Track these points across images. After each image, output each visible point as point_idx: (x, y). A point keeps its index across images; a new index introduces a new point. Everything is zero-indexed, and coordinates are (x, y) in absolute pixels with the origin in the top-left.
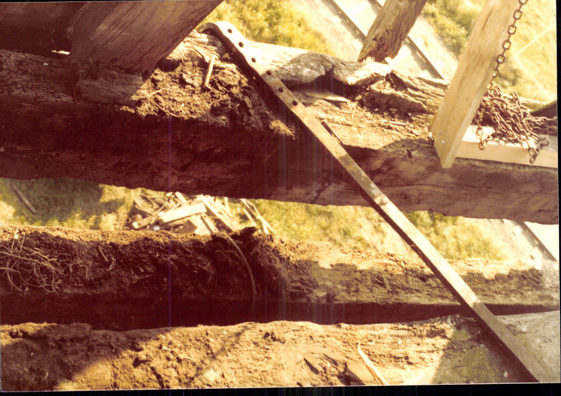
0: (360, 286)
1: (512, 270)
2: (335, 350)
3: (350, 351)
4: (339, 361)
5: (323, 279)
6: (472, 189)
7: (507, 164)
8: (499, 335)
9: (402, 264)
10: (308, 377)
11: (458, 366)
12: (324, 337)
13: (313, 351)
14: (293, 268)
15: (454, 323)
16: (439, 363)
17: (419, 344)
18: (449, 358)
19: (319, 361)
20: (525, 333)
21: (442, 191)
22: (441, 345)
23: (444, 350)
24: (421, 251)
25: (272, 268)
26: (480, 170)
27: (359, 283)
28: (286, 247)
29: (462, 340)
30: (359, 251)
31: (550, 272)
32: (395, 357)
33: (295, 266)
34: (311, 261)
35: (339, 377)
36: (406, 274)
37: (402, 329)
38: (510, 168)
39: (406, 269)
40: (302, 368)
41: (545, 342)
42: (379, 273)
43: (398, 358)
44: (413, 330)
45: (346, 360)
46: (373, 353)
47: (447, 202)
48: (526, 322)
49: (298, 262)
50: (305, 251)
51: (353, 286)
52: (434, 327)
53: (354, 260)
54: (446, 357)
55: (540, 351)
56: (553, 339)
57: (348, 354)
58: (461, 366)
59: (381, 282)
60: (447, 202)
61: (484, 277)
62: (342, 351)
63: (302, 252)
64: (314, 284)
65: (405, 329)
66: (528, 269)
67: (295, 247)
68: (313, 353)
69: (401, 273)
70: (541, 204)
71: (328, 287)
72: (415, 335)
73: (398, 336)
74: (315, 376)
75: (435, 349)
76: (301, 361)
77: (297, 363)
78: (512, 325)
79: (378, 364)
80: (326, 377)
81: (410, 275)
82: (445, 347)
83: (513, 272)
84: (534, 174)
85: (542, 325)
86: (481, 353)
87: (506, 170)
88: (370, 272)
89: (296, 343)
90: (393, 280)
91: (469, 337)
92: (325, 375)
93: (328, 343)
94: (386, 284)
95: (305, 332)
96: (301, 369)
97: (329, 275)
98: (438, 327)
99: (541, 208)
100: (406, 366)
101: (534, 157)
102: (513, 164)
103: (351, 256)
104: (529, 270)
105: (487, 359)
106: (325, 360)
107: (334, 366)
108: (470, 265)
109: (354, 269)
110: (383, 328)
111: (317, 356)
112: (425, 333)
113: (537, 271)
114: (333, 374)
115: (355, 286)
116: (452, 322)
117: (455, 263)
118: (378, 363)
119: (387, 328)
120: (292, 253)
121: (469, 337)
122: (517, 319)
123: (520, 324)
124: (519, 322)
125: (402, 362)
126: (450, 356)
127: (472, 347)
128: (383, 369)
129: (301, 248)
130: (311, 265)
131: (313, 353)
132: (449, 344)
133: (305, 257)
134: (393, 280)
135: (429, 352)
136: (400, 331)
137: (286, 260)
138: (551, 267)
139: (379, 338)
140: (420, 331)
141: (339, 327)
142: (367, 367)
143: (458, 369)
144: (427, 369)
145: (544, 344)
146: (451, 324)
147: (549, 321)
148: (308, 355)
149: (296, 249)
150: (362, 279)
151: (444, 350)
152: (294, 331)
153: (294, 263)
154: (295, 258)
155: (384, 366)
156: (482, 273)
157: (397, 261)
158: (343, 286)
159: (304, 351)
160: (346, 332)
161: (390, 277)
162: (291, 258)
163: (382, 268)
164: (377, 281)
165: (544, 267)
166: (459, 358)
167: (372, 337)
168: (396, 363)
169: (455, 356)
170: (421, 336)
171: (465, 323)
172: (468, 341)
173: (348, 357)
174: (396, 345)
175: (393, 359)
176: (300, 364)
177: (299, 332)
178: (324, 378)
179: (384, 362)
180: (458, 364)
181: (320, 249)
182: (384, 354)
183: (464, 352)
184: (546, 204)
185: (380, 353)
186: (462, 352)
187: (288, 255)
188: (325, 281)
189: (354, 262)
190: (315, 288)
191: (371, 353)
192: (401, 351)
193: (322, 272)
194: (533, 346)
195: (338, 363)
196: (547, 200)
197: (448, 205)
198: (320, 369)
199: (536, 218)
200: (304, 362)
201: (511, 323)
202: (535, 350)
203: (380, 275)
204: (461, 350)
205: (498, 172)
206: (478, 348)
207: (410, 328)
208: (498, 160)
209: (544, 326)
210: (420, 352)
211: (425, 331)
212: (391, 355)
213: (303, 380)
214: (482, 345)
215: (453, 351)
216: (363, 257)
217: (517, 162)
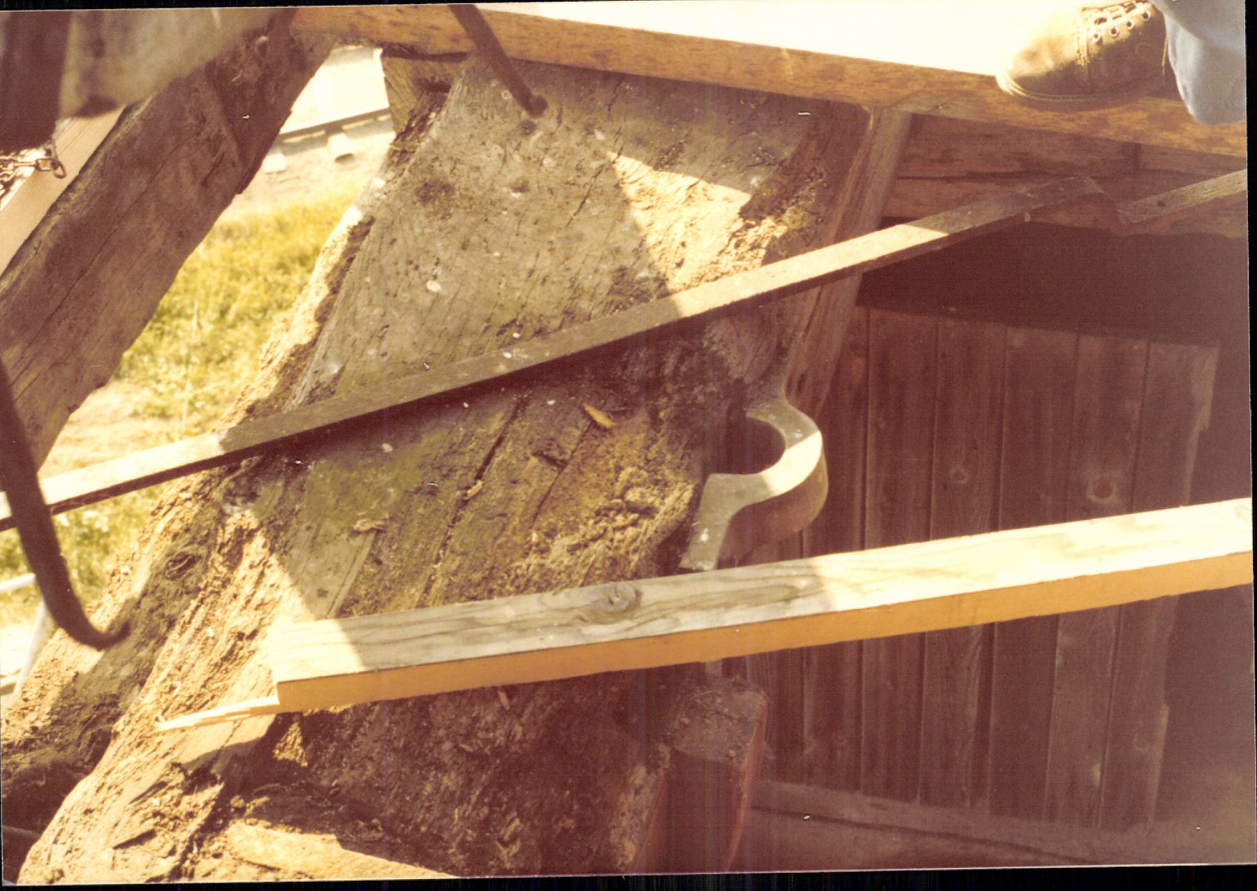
0: (167, 613)
1: (327, 277)
2: (139, 774)
3: (159, 743)
4: (162, 776)
5: (112, 678)
6: (64, 311)
7: (44, 221)
8: (306, 428)
9: (184, 495)
10: (148, 857)
11: (314, 538)
12: (103, 784)
13: (114, 821)
14: (56, 729)
15: (239, 500)
16: (287, 575)
17: (235, 596)
18: (291, 548)
19: (138, 818)
20: (342, 370)
21: (33, 376)
22: (260, 549)
23: (272, 551)
24: (68, 501)
25: (24, 778)
26: (23, 283)
27: (160, 610)
28: (11, 723)
29: (275, 502)
30: (113, 575)
31: (378, 199)
32: (225, 659)
33: (55, 723)
34: (69, 685)
35: (188, 790)
36: (204, 498)
37: (194, 613)
38: (56, 218)
39: (196, 494)
40: (126, 860)
41: (382, 338)
42: (168, 555)
43: (231, 652)
44: (207, 593)
45: (168, 759)
46: (190, 697)
47: (68, 372)
48: (325, 357)
49: (51, 713)
50: (42, 688)
51: (158, 625)
52: (223, 545)
53: (118, 596)
54: (285, 553)
55: (391, 358)
56: (388, 319)
57: (161, 751)
58: (318, 530)
59: (185, 562)
60: (68, 372)
61: (305, 346)
62: (148, 759)
63: (41, 696)
64: (108, 701)
65: (197, 608)
66: (345, 242)
67: (23, 704)
68: (116, 825)
69: (196, 508)
70: (186, 178)
71: (130, 677)
72: (218, 593)
73: (198, 630)
74: (155, 843)
75: (261, 568)
76: (114, 858)
77: (113, 866)
78: (314, 390)
79: (215, 699)
80: (171, 820)
81: (211, 490)
82: (269, 546)
83: (331, 279)
84: (102, 172)
85: (350, 328)
86: (321, 476)
87: (55, 228)
88: (157, 574)
89: (77, 850)
90: (197, 532)
91: (280, 484)
92: (166, 820)
93: (118, 782)
94: (195, 553)
95: (73, 819)
96: (126, 864)
97: (112, 664)
98: (227, 536)
99: (200, 179)
100: (254, 644)
101: (56, 164)
102: (53, 208)
103: (110, 596)
104: (349, 240)
105: (338, 471)
106: (144, 805)
107: (163, 790)
108: (270, 362)
109: (132, 605)
110: (172, 650)
111: (126, 817)
112: (224, 570)
113: (360, 223)
114: (174, 801)
115: (162, 620)
116: (234, 504)
117: (247, 391)
118: (213, 697)
119: (175, 641)
120: (31, 717)
121: (280, 484)
122: (309, 373)
123: (323, 372)
124: (316, 372)
125: (241, 648)
126: (289, 544)
127: (302, 490)
128: (227, 694)
129: (32, 694)
130: (74, 691)
131: (116, 825)
132: (266, 535)
133: (53, 694)
134: (197, 532)
135: (258, 583)
136: (193, 621)
137: (33, 737)
138: (372, 194)
139: (180, 669)
140: (215, 578)
141: (116, 734)
142: (198, 726)
143: (319, 539)
144: (282, 606)
145: (384, 344)
146: (236, 508)
147: (351, 310)
148: (113, 836)
149: (27, 705)
150: (159, 599)
151: (272, 551)
152: (55, 842)
153: (49, 722)
154: (41, 717)
155: (225, 688)
156: (295, 346)
157: (173, 505)
158: (147, 645)
159: (102, 841)
160: (129, 728)
161: (188, 536)
162: (39, 724)
163: (168, 542)
164: (180, 570)
165: (363, 206)
166: (304, 526)
167: (168, 683)
168: (237, 662)
169: (295, 535)
170: (226, 583)
171: (251, 479)
172: (285, 490)
173: (167, 754)
174: (211, 642)
175: (226, 665)
176: (118, 861)
177: (63, 833)
178: (172, 824)
179: (219, 684)
180: (310, 534)
181: (58, 655)
182: (205, 678)
183: (299, 510)
184: (194, 169)
185: (201, 683)
186: (297, 514)
187: (28, 727)
188: (117, 677)
189: (122, 600)
190: (115, 704)
191: (188, 703)
192: (223, 639)
193: (99, 673)
194: (374, 368)
195: (164, 779)
196: (184, 164)
197: (78, 371)
198: (149, 825)
199: (218, 197)
200: (119, 851)
201: (308, 389)
202: (383, 370)
203: (173, 557)
204: (293, 513)
205: (51, 245)
206: (309, 477)
207: (200, 596)
208: (26, 236)
209: (355, 323)
210: (248, 602)
211: (221, 568)
212: (216, 665)
213: (148, 871)
214: (310, 467)
215: (286, 532)
216: (126, 574)
217: (53, 199)
